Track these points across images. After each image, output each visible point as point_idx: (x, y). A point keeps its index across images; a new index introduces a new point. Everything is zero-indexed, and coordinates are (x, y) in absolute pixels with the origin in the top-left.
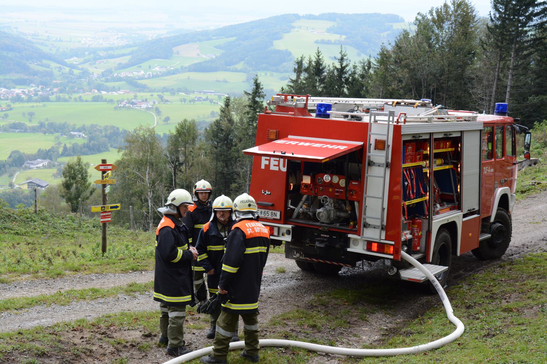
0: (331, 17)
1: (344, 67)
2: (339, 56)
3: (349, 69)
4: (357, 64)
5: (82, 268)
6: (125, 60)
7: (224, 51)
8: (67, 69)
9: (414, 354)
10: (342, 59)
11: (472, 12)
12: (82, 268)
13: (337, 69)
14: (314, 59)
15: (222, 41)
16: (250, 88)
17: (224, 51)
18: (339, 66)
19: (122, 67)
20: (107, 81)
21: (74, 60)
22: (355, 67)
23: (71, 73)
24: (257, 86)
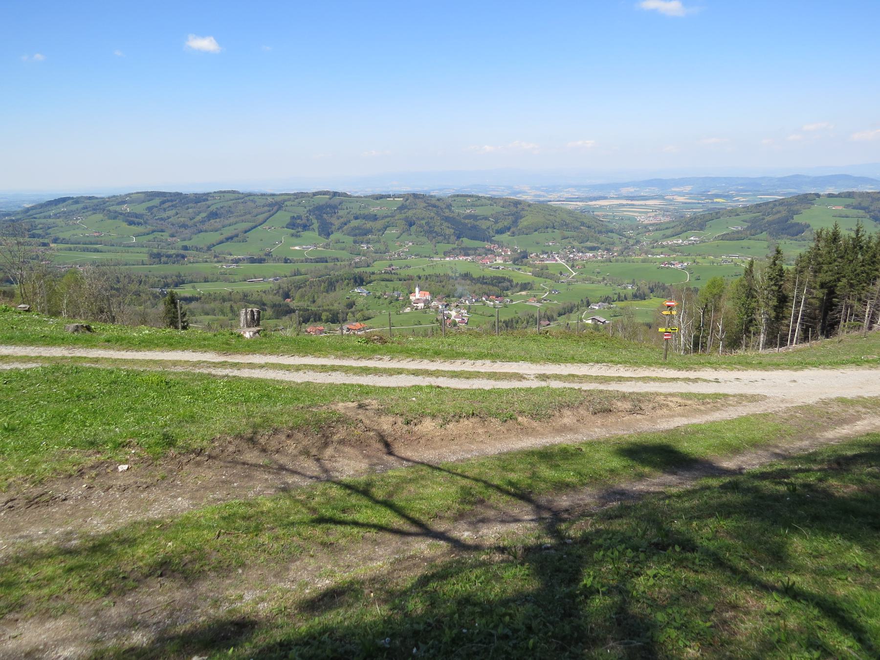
0: (850, 195)
1: (860, 237)
2: (855, 228)
3: (865, 239)
4: (873, 234)
5: (135, 441)
6: (669, 232)
7: (749, 224)
8: (624, 240)
9: (430, 466)
10: (858, 231)
11: (367, 375)
12: (135, 441)
13: (853, 239)
14: (831, 230)
15: (750, 216)
16: (772, 254)
17: (749, 224)
18: (854, 236)
19: (666, 237)
20: (653, 247)
21: (630, 233)
22: (870, 237)
23: (627, 242)
24: (778, 252)
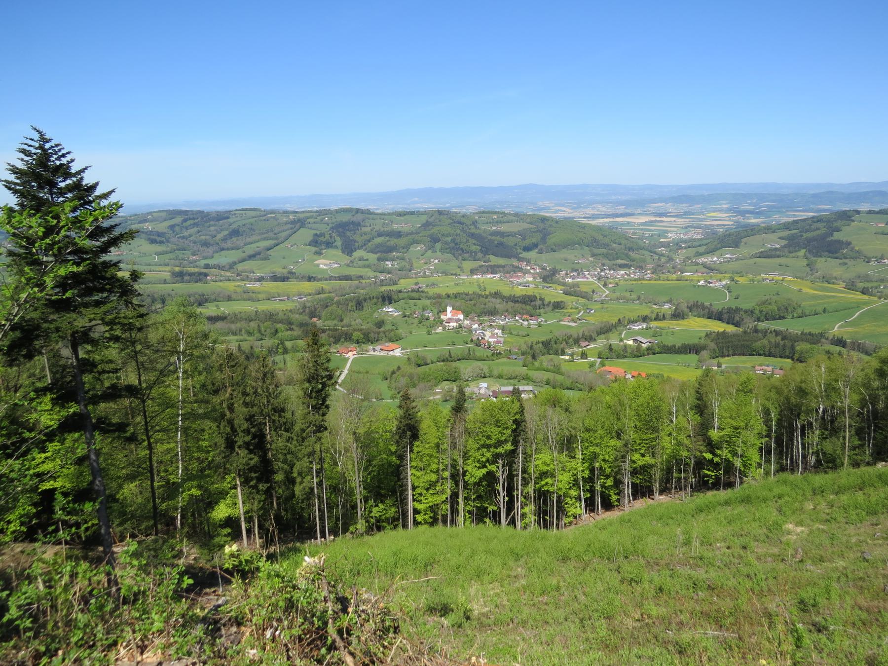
21: (663, 250)
